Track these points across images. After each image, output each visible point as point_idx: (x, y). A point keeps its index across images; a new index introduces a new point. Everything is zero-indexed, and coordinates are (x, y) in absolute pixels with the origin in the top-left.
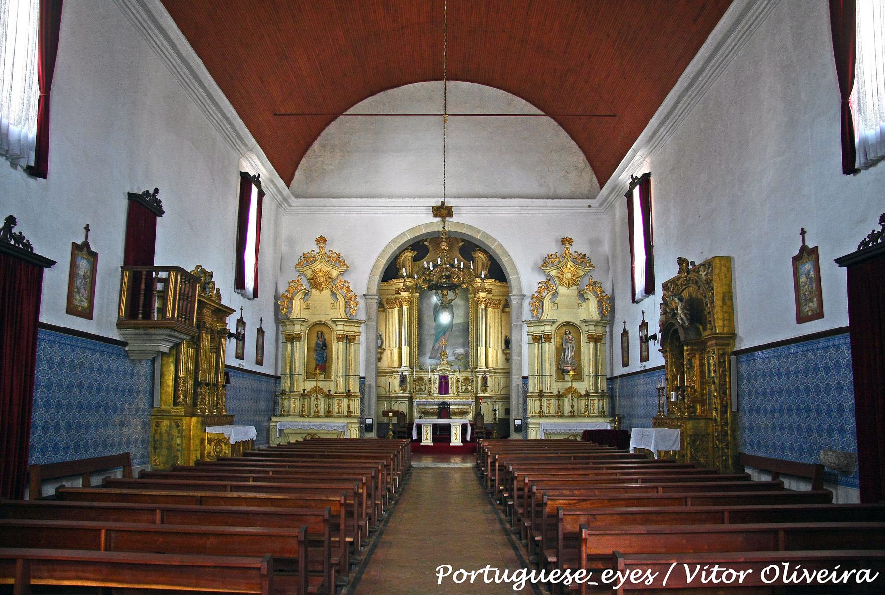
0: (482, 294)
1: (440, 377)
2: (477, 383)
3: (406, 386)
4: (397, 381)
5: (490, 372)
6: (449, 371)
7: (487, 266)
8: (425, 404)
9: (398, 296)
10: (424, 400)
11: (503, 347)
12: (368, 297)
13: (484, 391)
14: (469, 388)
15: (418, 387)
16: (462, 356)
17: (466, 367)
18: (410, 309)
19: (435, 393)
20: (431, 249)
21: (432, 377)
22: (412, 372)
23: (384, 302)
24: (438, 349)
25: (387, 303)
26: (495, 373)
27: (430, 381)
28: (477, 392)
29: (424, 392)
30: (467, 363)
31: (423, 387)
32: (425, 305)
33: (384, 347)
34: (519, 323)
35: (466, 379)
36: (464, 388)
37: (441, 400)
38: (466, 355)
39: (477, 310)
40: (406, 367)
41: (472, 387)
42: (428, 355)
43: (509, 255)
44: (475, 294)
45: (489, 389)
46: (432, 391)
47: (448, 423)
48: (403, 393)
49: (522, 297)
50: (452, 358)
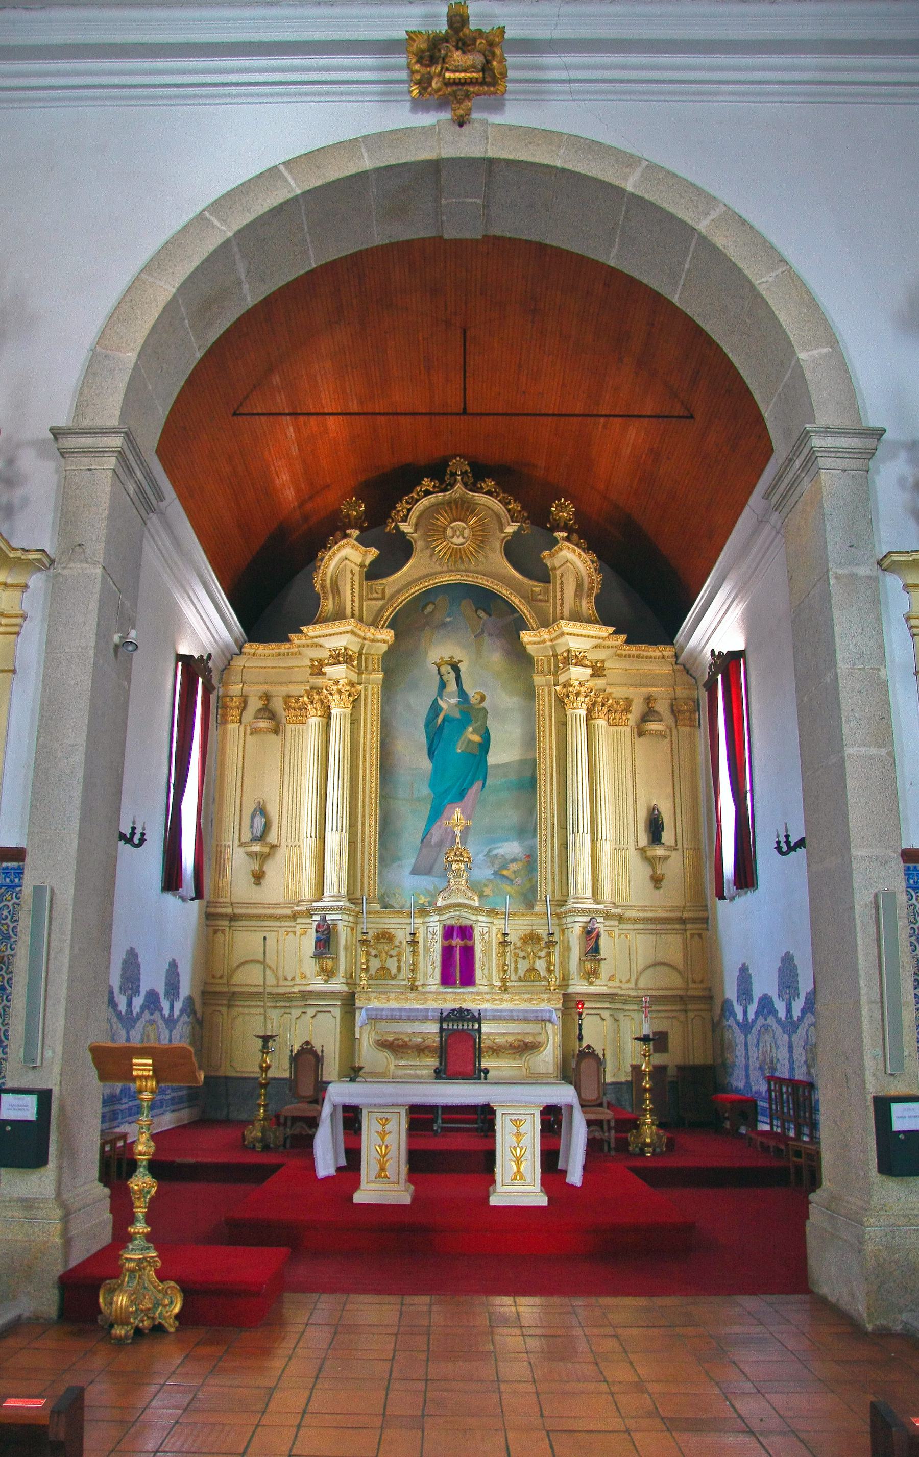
0: (577, 674)
1: (449, 932)
2: (568, 949)
3: (336, 959)
4: (309, 944)
5: (607, 916)
6: (477, 910)
7: (591, 589)
8: (395, 1017)
9: (319, 681)
10: (394, 1005)
11: (643, 840)
12: (70, 442)
13: (591, 975)
14: (541, 965)
15: (375, 964)
16: (514, 867)
17: (529, 898)
18: (354, 722)
19: (431, 981)
20: (419, 545)
21: (422, 930)
22: (358, 915)
23: (278, 704)
24: (441, 844)
25: (288, 707)
26: (620, 918)
27: (414, 943)
28: (565, 979)
29: (394, 978)
30: (533, 889)
31: (392, 965)
32: (400, 709)
33: (272, 838)
34: (863, 571)
35: (531, 938)
36: (523, 966)
37: (450, 1005)
38: (530, 862)
39: (563, 724)
40: (338, 897)
41: (549, 963)
42: (409, 862)
43: (783, 261)
44: (556, 674)
45: (605, 969)
46: (420, 976)
47: (480, 1100)
48: (326, 981)
49: (870, 443)
50: (484, 873)
